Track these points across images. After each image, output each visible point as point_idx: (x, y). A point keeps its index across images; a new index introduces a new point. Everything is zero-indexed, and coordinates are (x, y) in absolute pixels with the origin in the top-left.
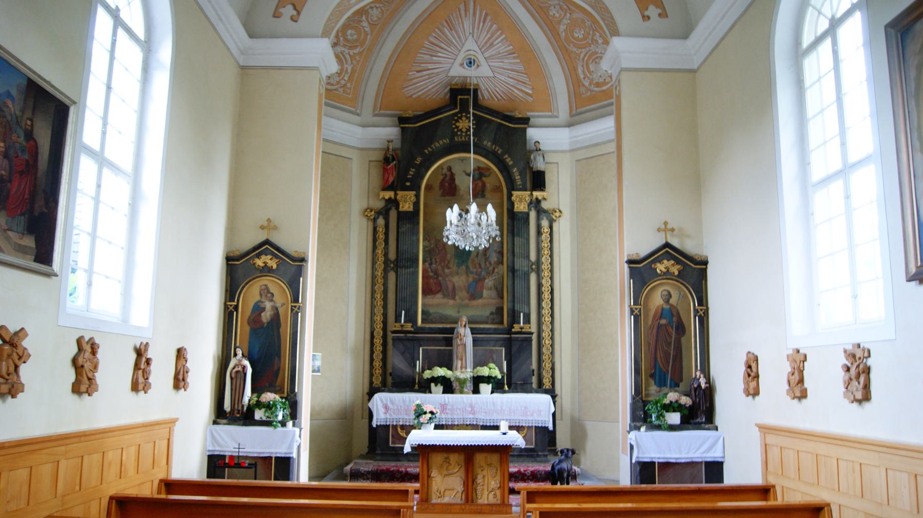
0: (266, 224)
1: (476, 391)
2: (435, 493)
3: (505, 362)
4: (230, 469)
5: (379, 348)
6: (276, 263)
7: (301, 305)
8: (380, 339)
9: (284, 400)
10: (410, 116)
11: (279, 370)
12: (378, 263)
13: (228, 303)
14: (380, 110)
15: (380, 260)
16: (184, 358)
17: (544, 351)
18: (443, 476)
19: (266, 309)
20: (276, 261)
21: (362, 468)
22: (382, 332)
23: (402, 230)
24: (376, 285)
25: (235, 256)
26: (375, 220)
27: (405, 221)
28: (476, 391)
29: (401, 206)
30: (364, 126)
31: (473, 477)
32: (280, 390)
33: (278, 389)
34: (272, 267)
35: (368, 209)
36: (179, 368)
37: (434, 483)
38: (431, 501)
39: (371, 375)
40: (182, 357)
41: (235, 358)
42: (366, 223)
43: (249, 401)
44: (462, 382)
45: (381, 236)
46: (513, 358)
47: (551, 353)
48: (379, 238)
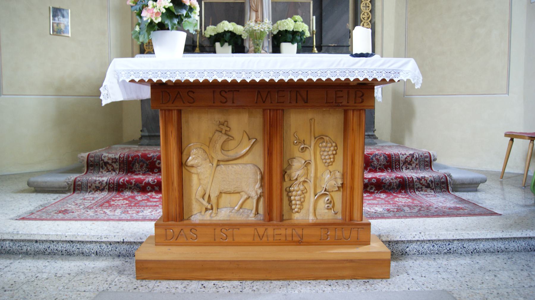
1: (276, 50)
2: (197, 200)
3: (314, 17)
17: (362, 8)
18: (215, 164)
21: (105, 154)
28: (276, 50)
31: (281, 165)
37: (195, 178)
38: (188, 219)
44: (255, 36)
46: (324, 14)
47: (371, 11)
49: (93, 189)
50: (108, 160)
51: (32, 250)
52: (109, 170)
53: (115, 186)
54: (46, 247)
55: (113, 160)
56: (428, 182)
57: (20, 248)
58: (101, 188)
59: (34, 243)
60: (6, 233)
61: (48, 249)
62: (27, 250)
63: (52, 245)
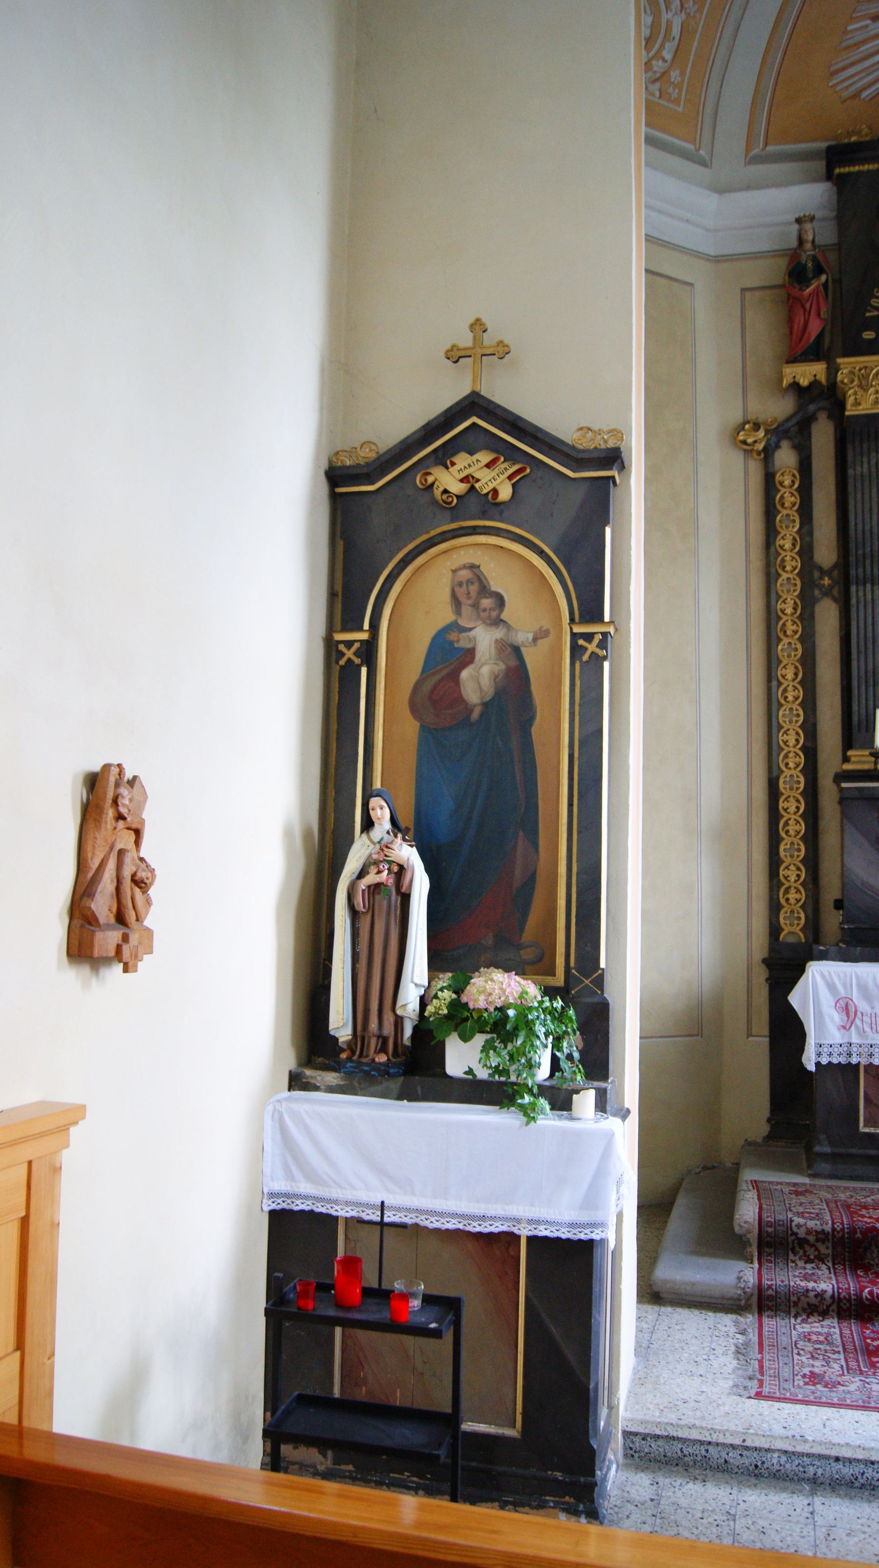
0: (466, 339)
4: (349, 1331)
5: (798, 827)
6: (510, 478)
7: (611, 630)
8: (798, 801)
9: (558, 1004)
10: (862, 139)
11: (531, 879)
12: (785, 576)
13: (339, 637)
14: (766, 144)
15: (788, 568)
16: (120, 817)
19: (478, 655)
20: (511, 471)
22: (802, 779)
23: (858, 469)
24: (779, 640)
25: (358, 465)
26: (767, 454)
27: (865, 446)
29: (850, 401)
30: (721, 190)
32: (540, 959)
33: (528, 954)
34: (495, 492)
35: (744, 424)
36: (95, 864)
39: (774, 907)
40: (110, 813)
41: (364, 836)
42: (741, 465)
43: (423, 1002)
45: (789, 498)
48: (783, 505)
49: (804, 1310)
50: (806, 1234)
51: (826, 1476)
52: (808, 1256)
53: (853, 1308)
54: (857, 1473)
55: (819, 1236)
56: (801, 1252)
57: (801, 1469)
58: (820, 1310)
59: (831, 1461)
60: (781, 1438)
61: (859, 1477)
62: (815, 1474)
63: (870, 1470)
